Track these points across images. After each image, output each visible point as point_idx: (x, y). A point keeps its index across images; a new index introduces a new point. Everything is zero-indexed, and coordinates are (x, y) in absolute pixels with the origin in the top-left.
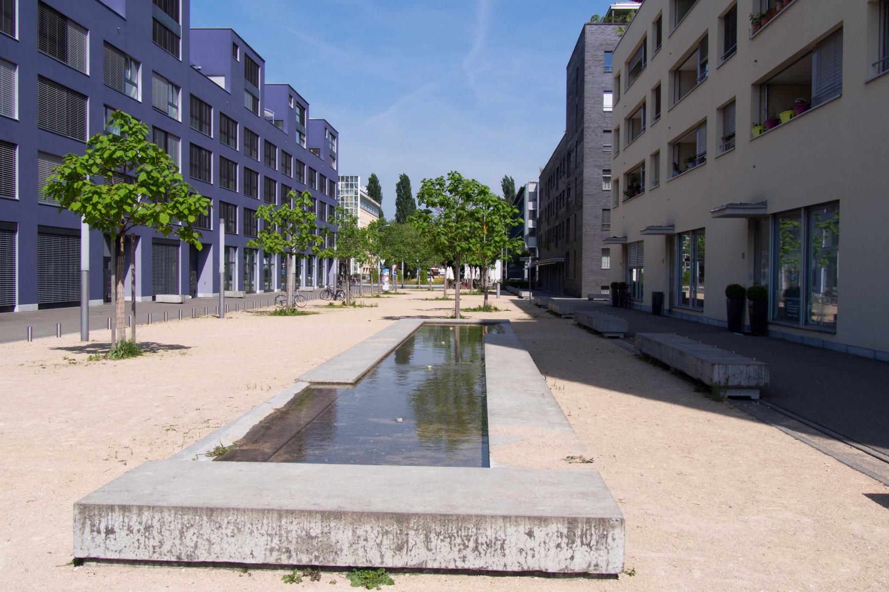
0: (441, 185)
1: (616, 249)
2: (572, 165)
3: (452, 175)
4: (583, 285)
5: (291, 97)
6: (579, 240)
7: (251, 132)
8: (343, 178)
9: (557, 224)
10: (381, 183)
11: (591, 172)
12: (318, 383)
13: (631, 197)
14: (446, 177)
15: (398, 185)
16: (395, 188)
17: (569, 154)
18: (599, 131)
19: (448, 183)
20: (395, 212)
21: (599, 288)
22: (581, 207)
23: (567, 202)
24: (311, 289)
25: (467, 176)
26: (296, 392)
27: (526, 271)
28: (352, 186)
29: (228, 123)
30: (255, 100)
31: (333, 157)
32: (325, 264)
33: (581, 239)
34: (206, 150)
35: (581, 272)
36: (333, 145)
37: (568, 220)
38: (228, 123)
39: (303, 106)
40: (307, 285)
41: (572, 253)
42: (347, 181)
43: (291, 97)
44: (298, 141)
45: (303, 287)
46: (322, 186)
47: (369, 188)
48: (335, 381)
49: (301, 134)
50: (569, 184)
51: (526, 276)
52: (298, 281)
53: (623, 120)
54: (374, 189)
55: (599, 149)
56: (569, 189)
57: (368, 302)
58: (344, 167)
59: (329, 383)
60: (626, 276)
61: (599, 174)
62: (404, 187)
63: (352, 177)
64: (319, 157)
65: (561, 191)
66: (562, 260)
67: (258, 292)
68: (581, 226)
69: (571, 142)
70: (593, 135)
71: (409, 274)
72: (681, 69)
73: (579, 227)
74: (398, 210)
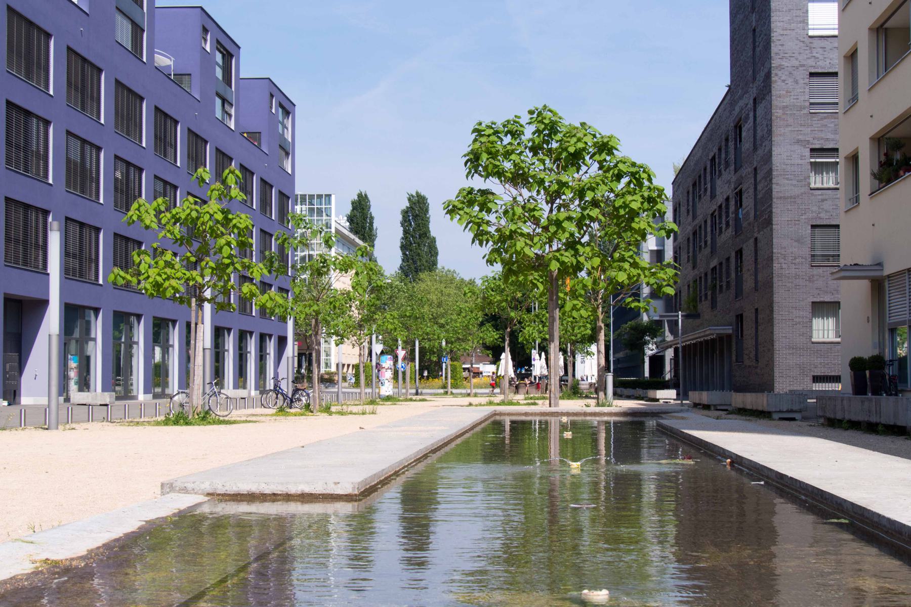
0: (515, 134)
1: (854, 294)
2: (747, 145)
3: (537, 115)
4: (777, 374)
5: (205, 30)
6: (765, 287)
7: (130, 91)
8: (303, 197)
9: (714, 263)
10: (374, 211)
11: (788, 153)
12: (237, 497)
13: (889, 181)
14: (525, 119)
15: (405, 213)
16: (400, 218)
17: (738, 128)
18: (802, 75)
19: (529, 132)
20: (399, 262)
21: (809, 379)
22: (769, 222)
23: (737, 219)
24: (242, 393)
25: (569, 118)
26: (152, 515)
27: (647, 360)
28: (320, 212)
29: (83, 73)
30: (137, 30)
31: (286, 150)
32: (271, 347)
33: (769, 285)
34: (39, 118)
35: (771, 350)
36: (285, 127)
37: (739, 253)
38: (83, 73)
39: (228, 51)
40: (236, 387)
41: (749, 316)
42: (311, 203)
43: (205, 30)
44: (219, 114)
45: (229, 390)
46: (265, 203)
47: (351, 219)
48: (294, 489)
49: (224, 101)
50: (739, 182)
51: (647, 374)
52: (218, 373)
53: (867, 31)
54: (361, 218)
55: (802, 108)
56: (740, 194)
57: (355, 409)
58: (309, 172)
59: (274, 497)
60: (881, 345)
61: (802, 157)
62: (415, 217)
63: (320, 197)
64: (259, 148)
65: (720, 199)
66: (729, 330)
67: (141, 397)
68: (770, 259)
69: (741, 103)
70: (790, 81)
71: (429, 368)
72: (886, 26)
73: (764, 260)
74: (405, 259)
